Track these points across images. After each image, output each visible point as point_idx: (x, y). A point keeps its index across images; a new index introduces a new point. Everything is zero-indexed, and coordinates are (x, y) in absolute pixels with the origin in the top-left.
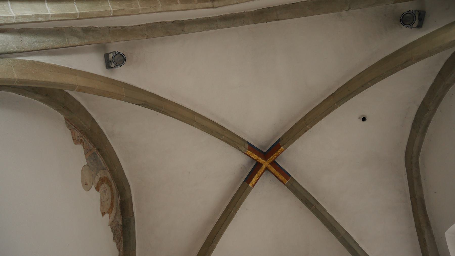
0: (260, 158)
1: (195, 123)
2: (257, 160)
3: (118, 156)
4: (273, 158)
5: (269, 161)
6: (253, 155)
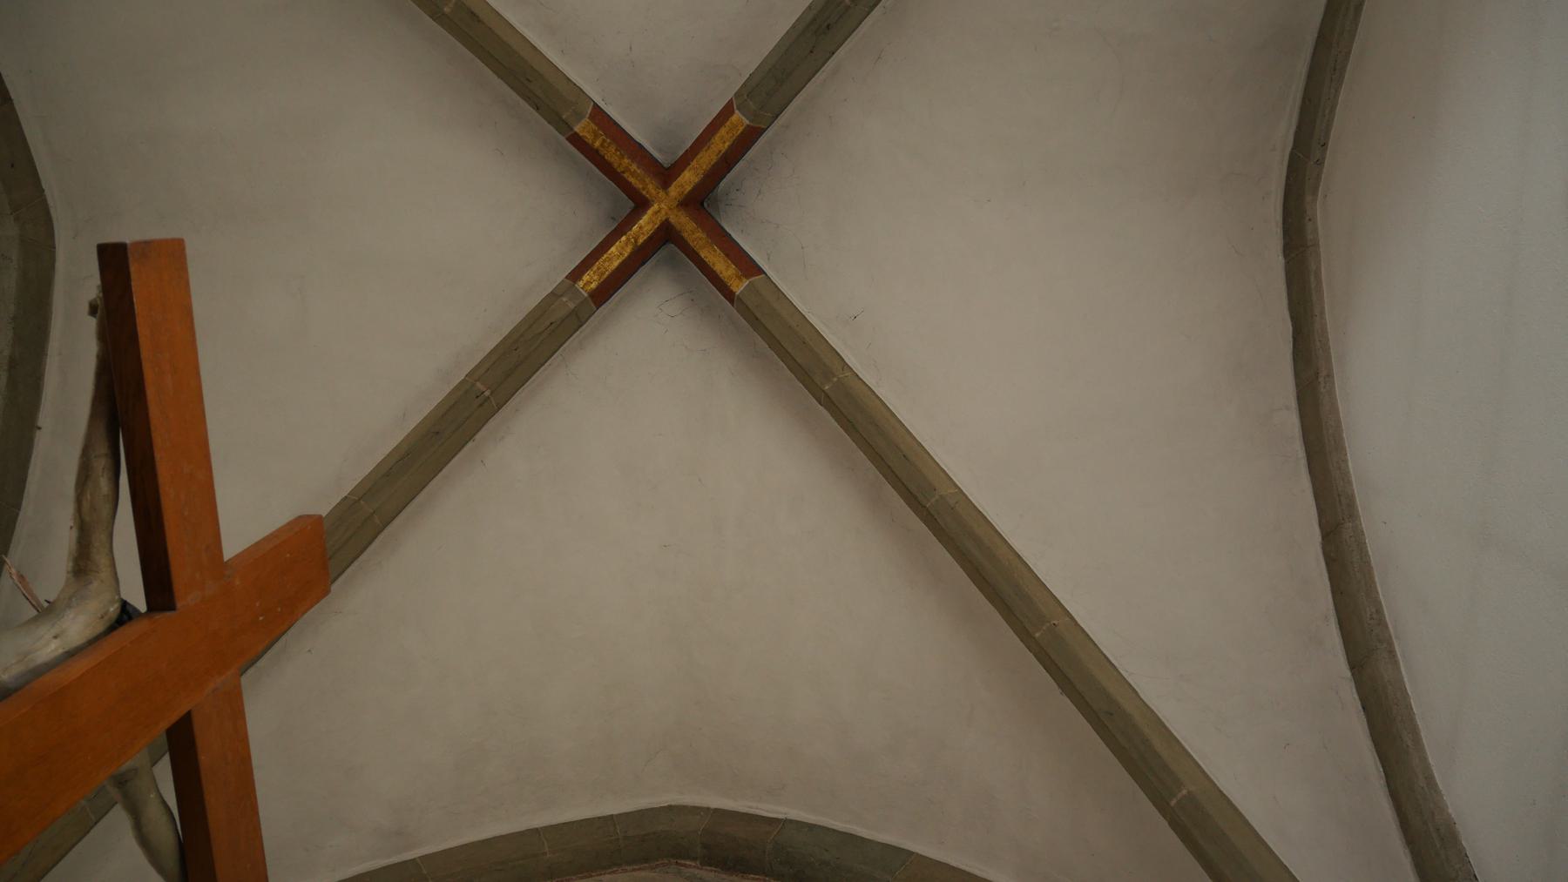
0: (631, 229)
1: (362, 502)
2: (639, 244)
3: (504, 833)
4: (633, 174)
5: (653, 191)
6: (610, 259)
